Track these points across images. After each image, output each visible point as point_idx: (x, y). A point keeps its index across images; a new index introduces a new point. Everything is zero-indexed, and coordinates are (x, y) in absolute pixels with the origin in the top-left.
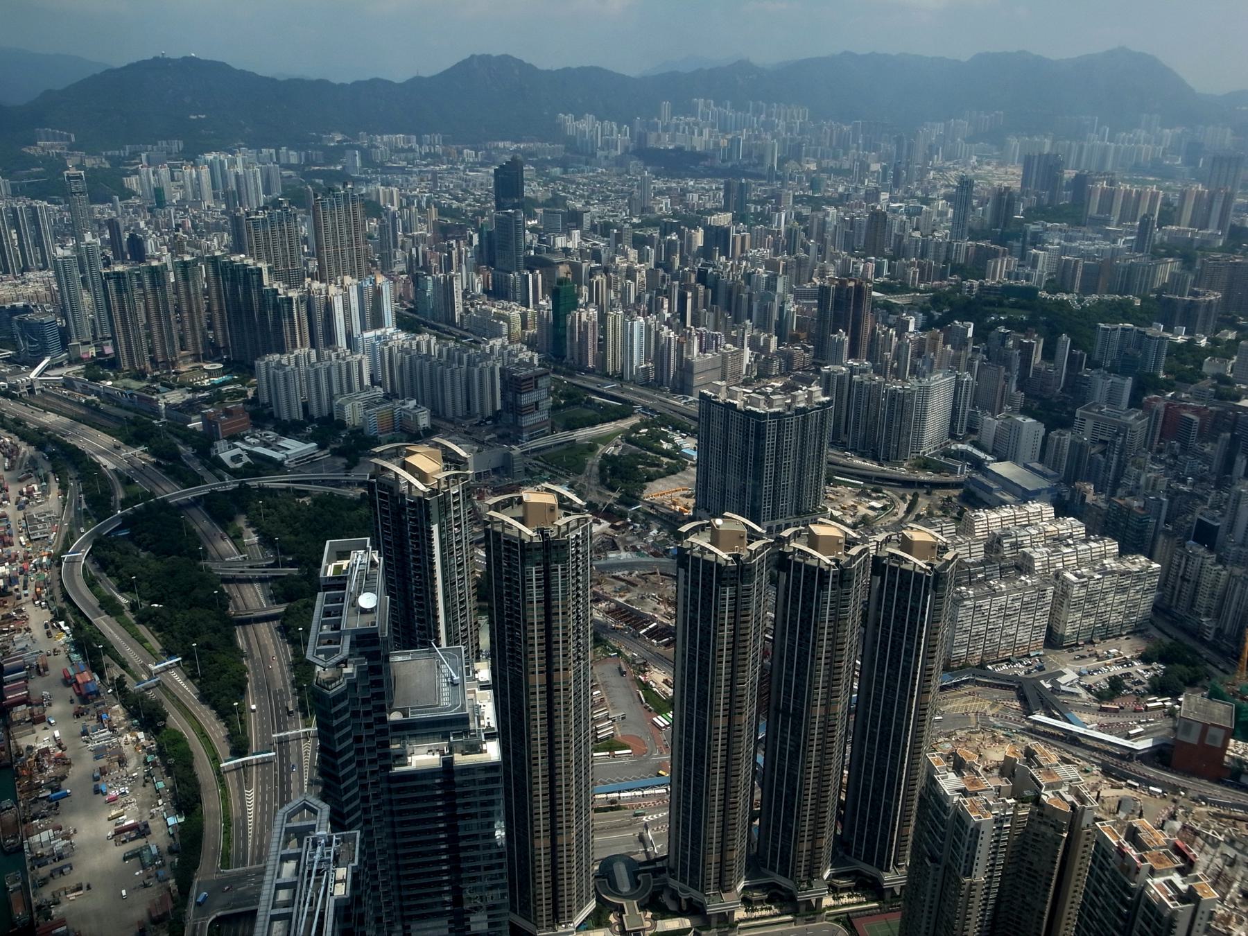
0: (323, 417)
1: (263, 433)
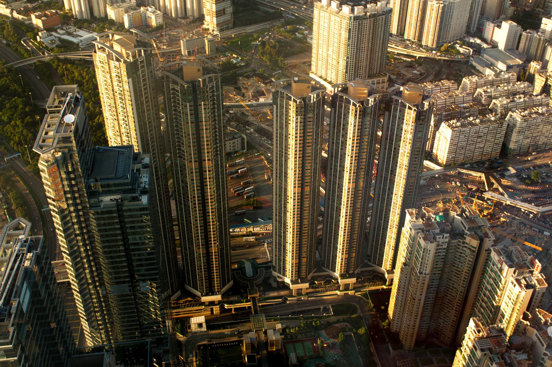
0: (102, 18)
1: (68, 27)
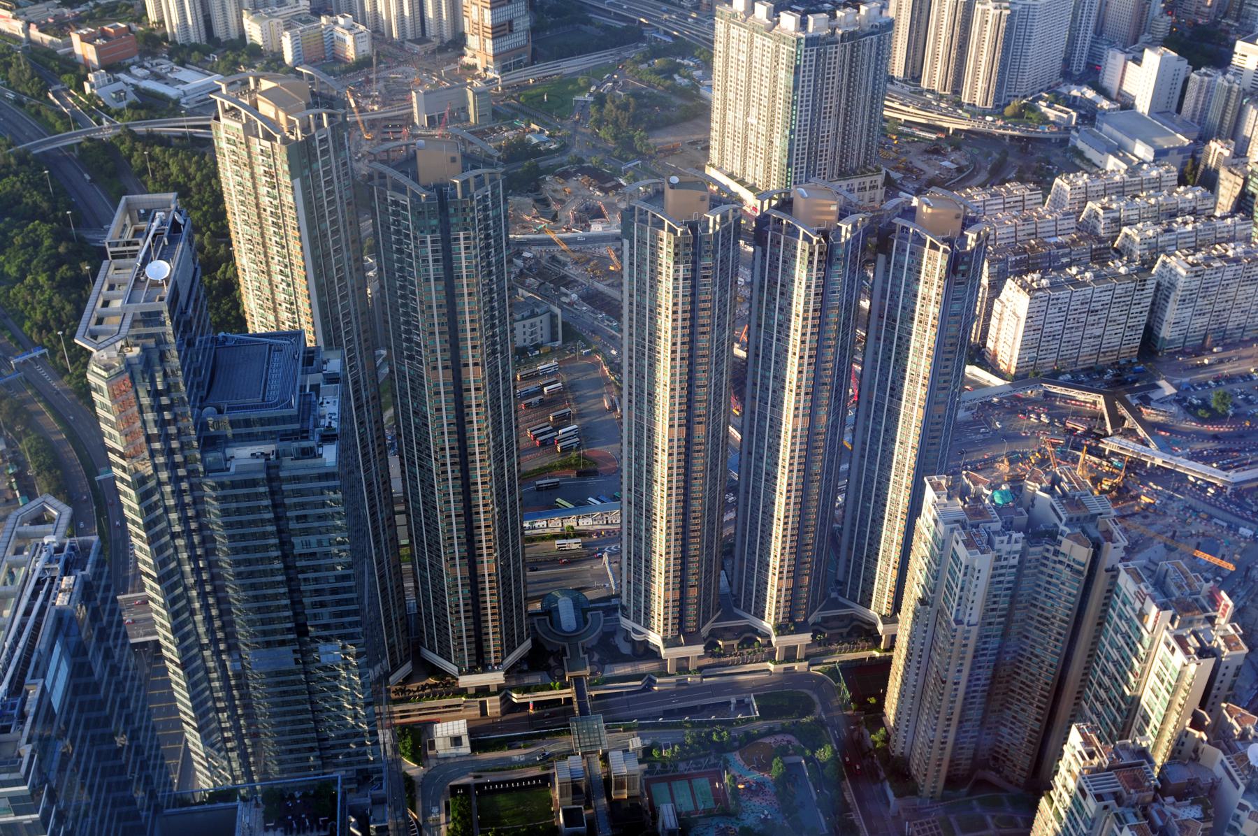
1: (154, 62)
